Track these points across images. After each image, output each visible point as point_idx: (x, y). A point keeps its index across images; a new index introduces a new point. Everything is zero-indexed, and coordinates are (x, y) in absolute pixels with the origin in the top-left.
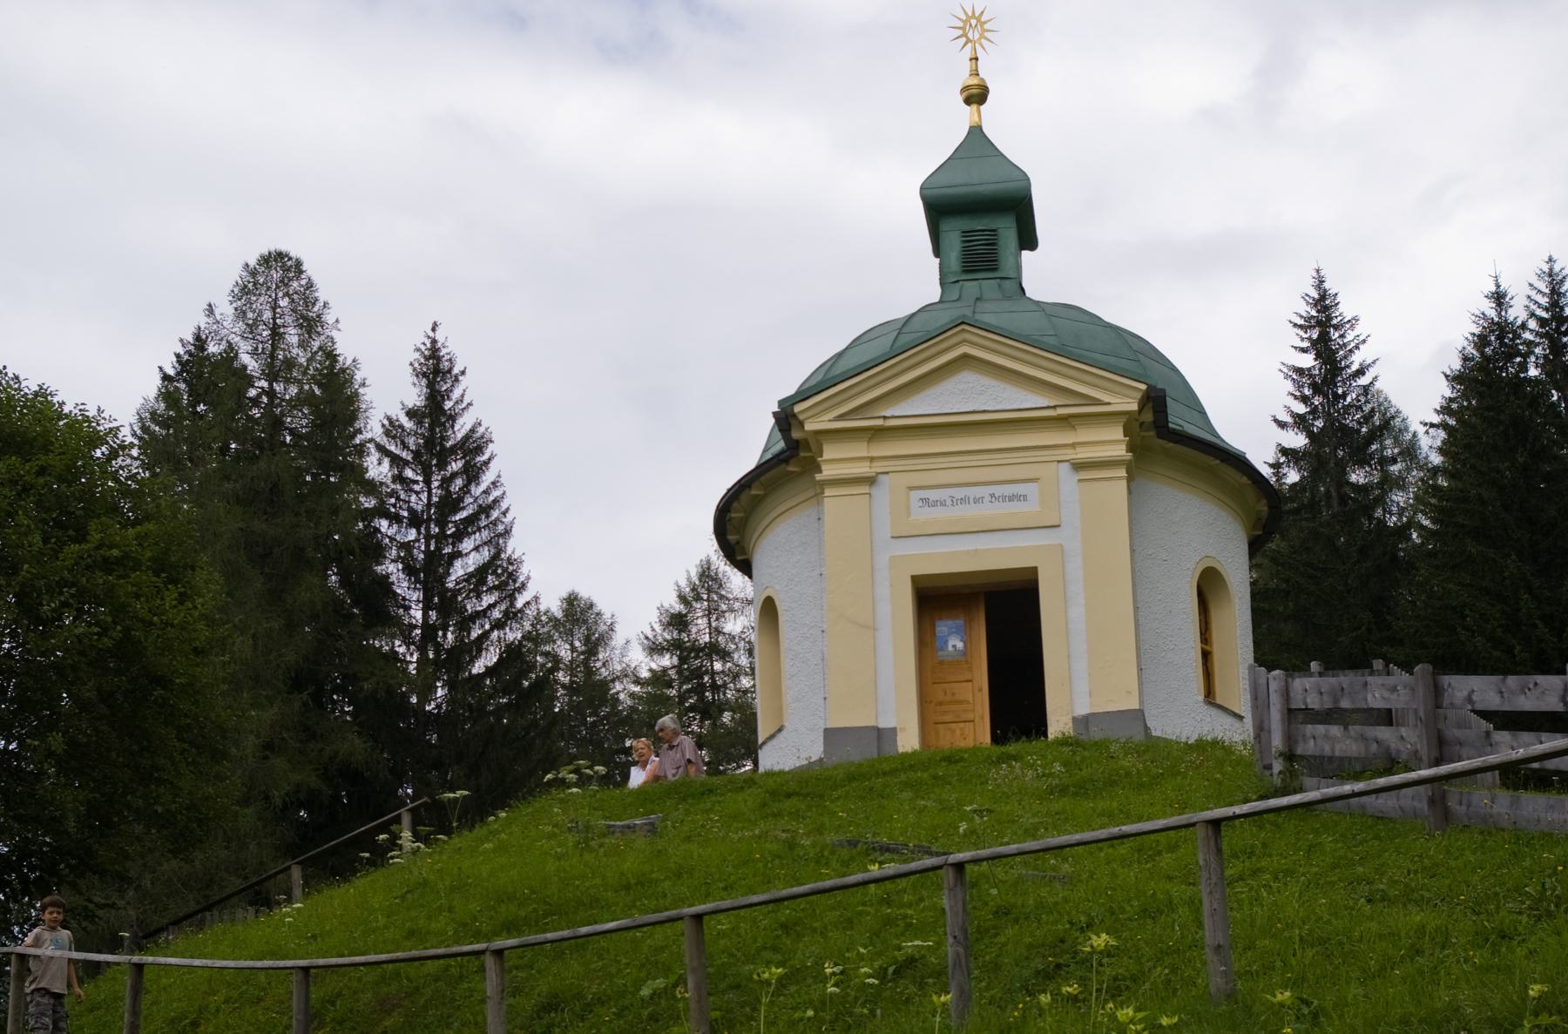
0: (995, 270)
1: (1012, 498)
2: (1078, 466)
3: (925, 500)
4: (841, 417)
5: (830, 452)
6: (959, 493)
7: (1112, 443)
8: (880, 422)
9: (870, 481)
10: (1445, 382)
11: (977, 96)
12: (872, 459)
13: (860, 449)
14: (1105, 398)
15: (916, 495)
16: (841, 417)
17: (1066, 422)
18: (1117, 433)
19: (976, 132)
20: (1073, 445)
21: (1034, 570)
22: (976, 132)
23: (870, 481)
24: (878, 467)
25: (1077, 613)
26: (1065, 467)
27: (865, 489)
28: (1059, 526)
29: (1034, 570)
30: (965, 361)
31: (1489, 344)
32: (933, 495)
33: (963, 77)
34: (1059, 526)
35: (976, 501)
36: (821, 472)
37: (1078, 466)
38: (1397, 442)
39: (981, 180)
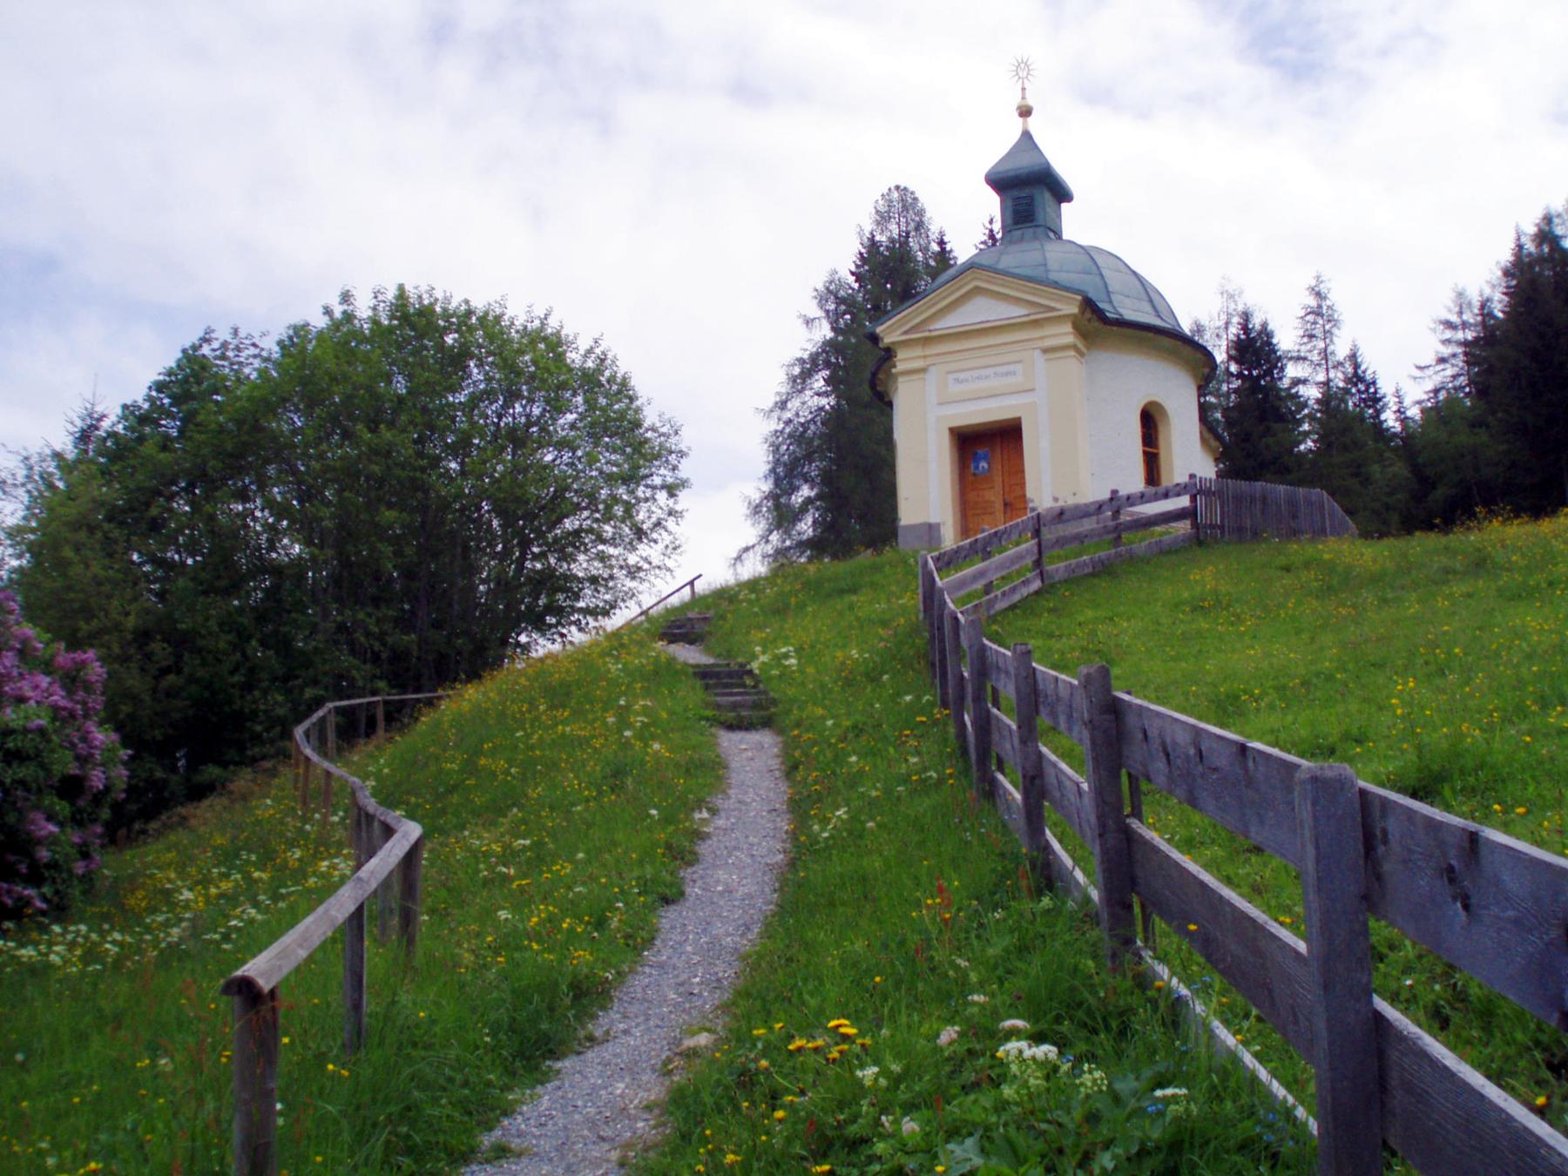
0: (1032, 221)
1: (1007, 374)
2: (1045, 351)
3: (957, 380)
4: (906, 333)
5: (901, 355)
6: (976, 373)
7: (1065, 334)
8: (927, 334)
9: (923, 370)
10: (685, 477)
11: (1025, 112)
12: (925, 357)
13: (918, 352)
14: (1058, 306)
15: (951, 377)
16: (906, 333)
17: (1036, 323)
18: (1068, 328)
19: (1027, 135)
20: (1042, 338)
21: (1019, 419)
22: (1027, 135)
23: (923, 370)
24: (929, 361)
25: (1044, 444)
26: (1037, 353)
27: (921, 376)
28: (1033, 390)
29: (1019, 419)
30: (977, 291)
31: (864, 1010)
32: (962, 376)
33: (1016, 100)
34: (1033, 390)
35: (987, 377)
36: (895, 366)
37: (1045, 351)
38: (772, 667)
39: (1025, 163)
